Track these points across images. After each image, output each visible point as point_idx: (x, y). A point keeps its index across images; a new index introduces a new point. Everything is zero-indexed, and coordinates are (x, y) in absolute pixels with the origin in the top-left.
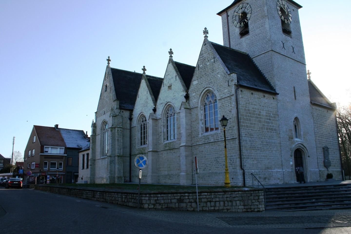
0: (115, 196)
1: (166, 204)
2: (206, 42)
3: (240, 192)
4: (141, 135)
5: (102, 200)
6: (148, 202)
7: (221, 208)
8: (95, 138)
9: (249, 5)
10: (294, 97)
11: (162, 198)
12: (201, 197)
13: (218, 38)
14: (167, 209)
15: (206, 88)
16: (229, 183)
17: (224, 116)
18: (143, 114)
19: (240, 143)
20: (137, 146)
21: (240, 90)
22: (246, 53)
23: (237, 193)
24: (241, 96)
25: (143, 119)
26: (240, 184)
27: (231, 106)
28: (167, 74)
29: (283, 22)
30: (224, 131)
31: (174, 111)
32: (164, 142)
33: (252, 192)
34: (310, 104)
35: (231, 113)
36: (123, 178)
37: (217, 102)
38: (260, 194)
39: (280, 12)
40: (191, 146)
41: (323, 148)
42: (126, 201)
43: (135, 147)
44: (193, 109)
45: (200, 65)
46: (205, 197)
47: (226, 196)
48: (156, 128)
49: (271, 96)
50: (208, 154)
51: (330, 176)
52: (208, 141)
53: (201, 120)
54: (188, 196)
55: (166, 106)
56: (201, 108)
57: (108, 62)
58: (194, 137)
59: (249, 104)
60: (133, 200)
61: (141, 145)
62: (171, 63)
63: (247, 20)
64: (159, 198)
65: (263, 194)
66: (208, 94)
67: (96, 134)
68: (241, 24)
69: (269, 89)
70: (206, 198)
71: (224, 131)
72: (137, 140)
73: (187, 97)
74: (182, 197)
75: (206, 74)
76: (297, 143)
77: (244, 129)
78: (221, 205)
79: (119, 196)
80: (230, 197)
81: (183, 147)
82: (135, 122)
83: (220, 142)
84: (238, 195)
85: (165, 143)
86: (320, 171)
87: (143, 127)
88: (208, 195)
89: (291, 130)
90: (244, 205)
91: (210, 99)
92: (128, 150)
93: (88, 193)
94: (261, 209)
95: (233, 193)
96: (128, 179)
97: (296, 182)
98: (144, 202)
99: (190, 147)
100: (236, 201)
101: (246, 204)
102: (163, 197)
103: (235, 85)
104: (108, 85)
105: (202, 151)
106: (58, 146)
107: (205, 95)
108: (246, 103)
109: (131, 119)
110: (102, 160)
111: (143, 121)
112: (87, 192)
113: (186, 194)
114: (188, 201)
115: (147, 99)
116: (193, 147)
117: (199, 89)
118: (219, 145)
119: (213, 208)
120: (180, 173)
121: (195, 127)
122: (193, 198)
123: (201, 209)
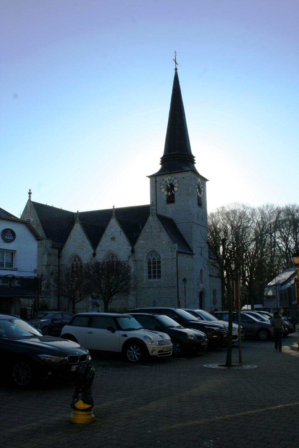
9: (176, 180)
15: (152, 248)
19: (178, 289)
22: (171, 218)
27: (173, 265)
41: (213, 290)
45: (147, 230)
49: (190, 256)
52: (152, 286)
53: (146, 270)
57: (31, 195)
63: (174, 192)
66: (153, 252)
68: (168, 193)
73: (133, 251)
75: (152, 238)
86: (211, 307)
89: (198, 278)
115: (84, 242)
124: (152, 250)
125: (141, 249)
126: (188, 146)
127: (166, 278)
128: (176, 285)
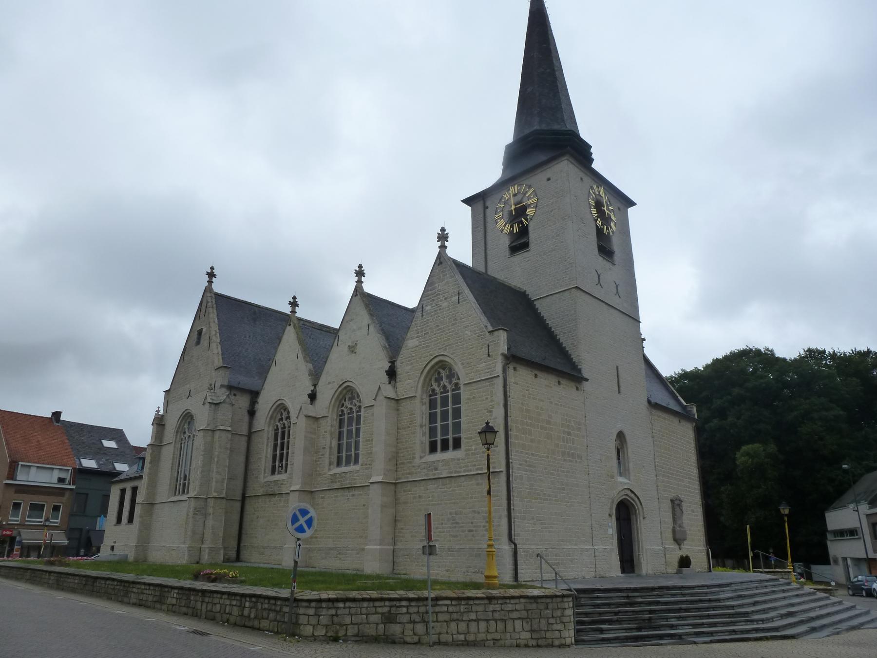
0: (222, 601)
1: (356, 627)
2: (442, 259)
3: (522, 600)
4: (275, 449)
5: (184, 610)
6: (314, 621)
7: (481, 637)
8: (160, 452)
10: (617, 388)
11: (347, 611)
12: (437, 609)
13: (462, 250)
14: (357, 639)
16: (495, 577)
17: (487, 423)
18: (282, 404)
20: (262, 476)
21: (511, 367)
23: (517, 601)
24: (513, 380)
25: (282, 414)
26: (507, 578)
28: (347, 319)
29: (599, 231)
30: (488, 456)
31: (360, 401)
32: (330, 469)
33: (549, 600)
34: (646, 403)
35: (491, 416)
36: (222, 552)
37: (459, 389)
38: (566, 605)
39: (594, 211)
40: (395, 484)
41: (672, 501)
42: (252, 616)
43: (257, 477)
44: (408, 402)
46: (445, 609)
47: (491, 607)
48: (313, 436)
49: (573, 384)
50: (433, 505)
51: (685, 562)
54: (407, 607)
55: (340, 389)
56: (422, 399)
58: (403, 463)
59: (529, 397)
60: (272, 615)
61: (273, 473)
62: (358, 297)
64: (339, 612)
65: (571, 605)
66: (441, 370)
67: (161, 442)
68: (512, 227)
69: (568, 371)
70: (447, 612)
71: (488, 456)
72: (263, 462)
74: (394, 609)
76: (620, 489)
77: (517, 452)
78: (480, 631)
79: (234, 603)
80: (502, 610)
81: (376, 485)
82: (262, 421)
83: (463, 479)
84: (518, 607)
85: (333, 472)
87: (280, 431)
88: (452, 605)
90: (532, 631)
91: (445, 382)
92: (239, 483)
93: (147, 592)
94: (568, 641)
95: (508, 601)
96: (233, 554)
97: (619, 574)
98: (303, 620)
99: (394, 486)
100: (514, 619)
101: (535, 627)
102: (350, 608)
103: (503, 354)
104: (204, 330)
105: (420, 497)
106: (53, 464)
107: (432, 371)
108: (524, 396)
109: (252, 413)
110: (172, 504)
111: (281, 419)
112: (143, 587)
113: (404, 603)
114: (405, 619)
116: (399, 486)
117: (421, 358)
118: (461, 486)
119: (462, 637)
120: (367, 544)
121: (407, 441)
122: (418, 612)
123: (435, 638)
124: (437, 363)
125: (412, 364)
126: (560, 87)
127: (473, 447)
128: (503, 468)
